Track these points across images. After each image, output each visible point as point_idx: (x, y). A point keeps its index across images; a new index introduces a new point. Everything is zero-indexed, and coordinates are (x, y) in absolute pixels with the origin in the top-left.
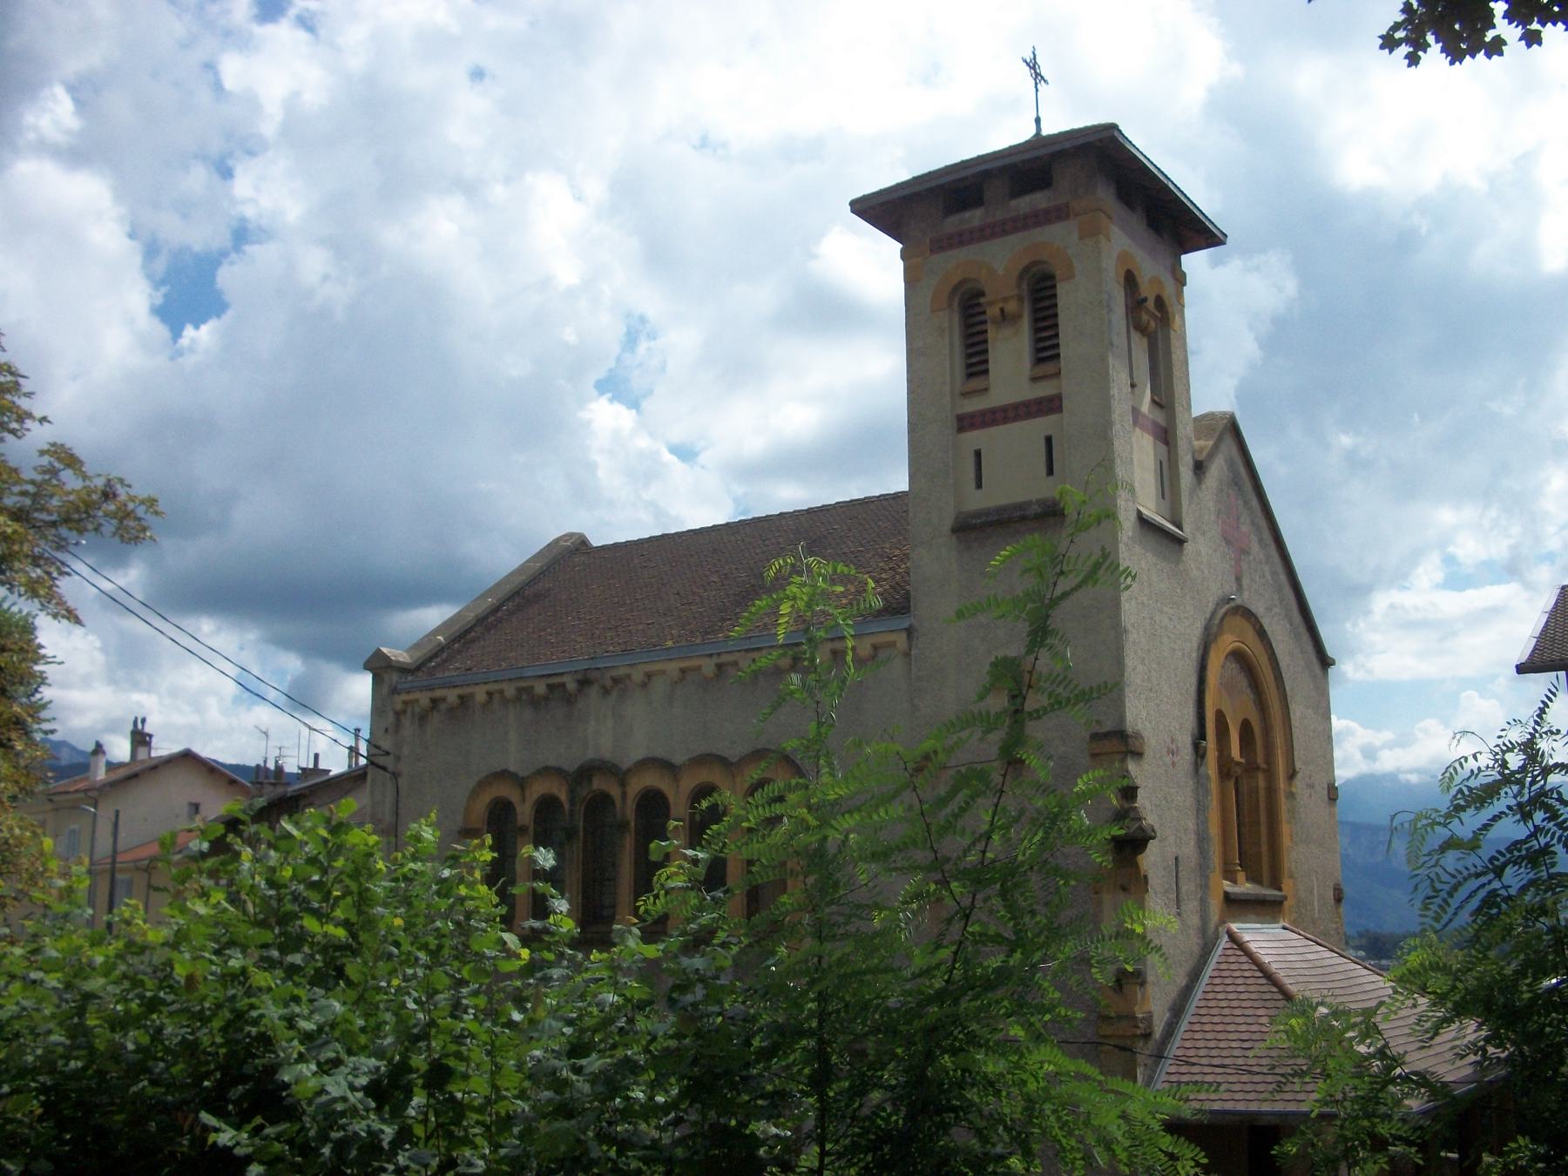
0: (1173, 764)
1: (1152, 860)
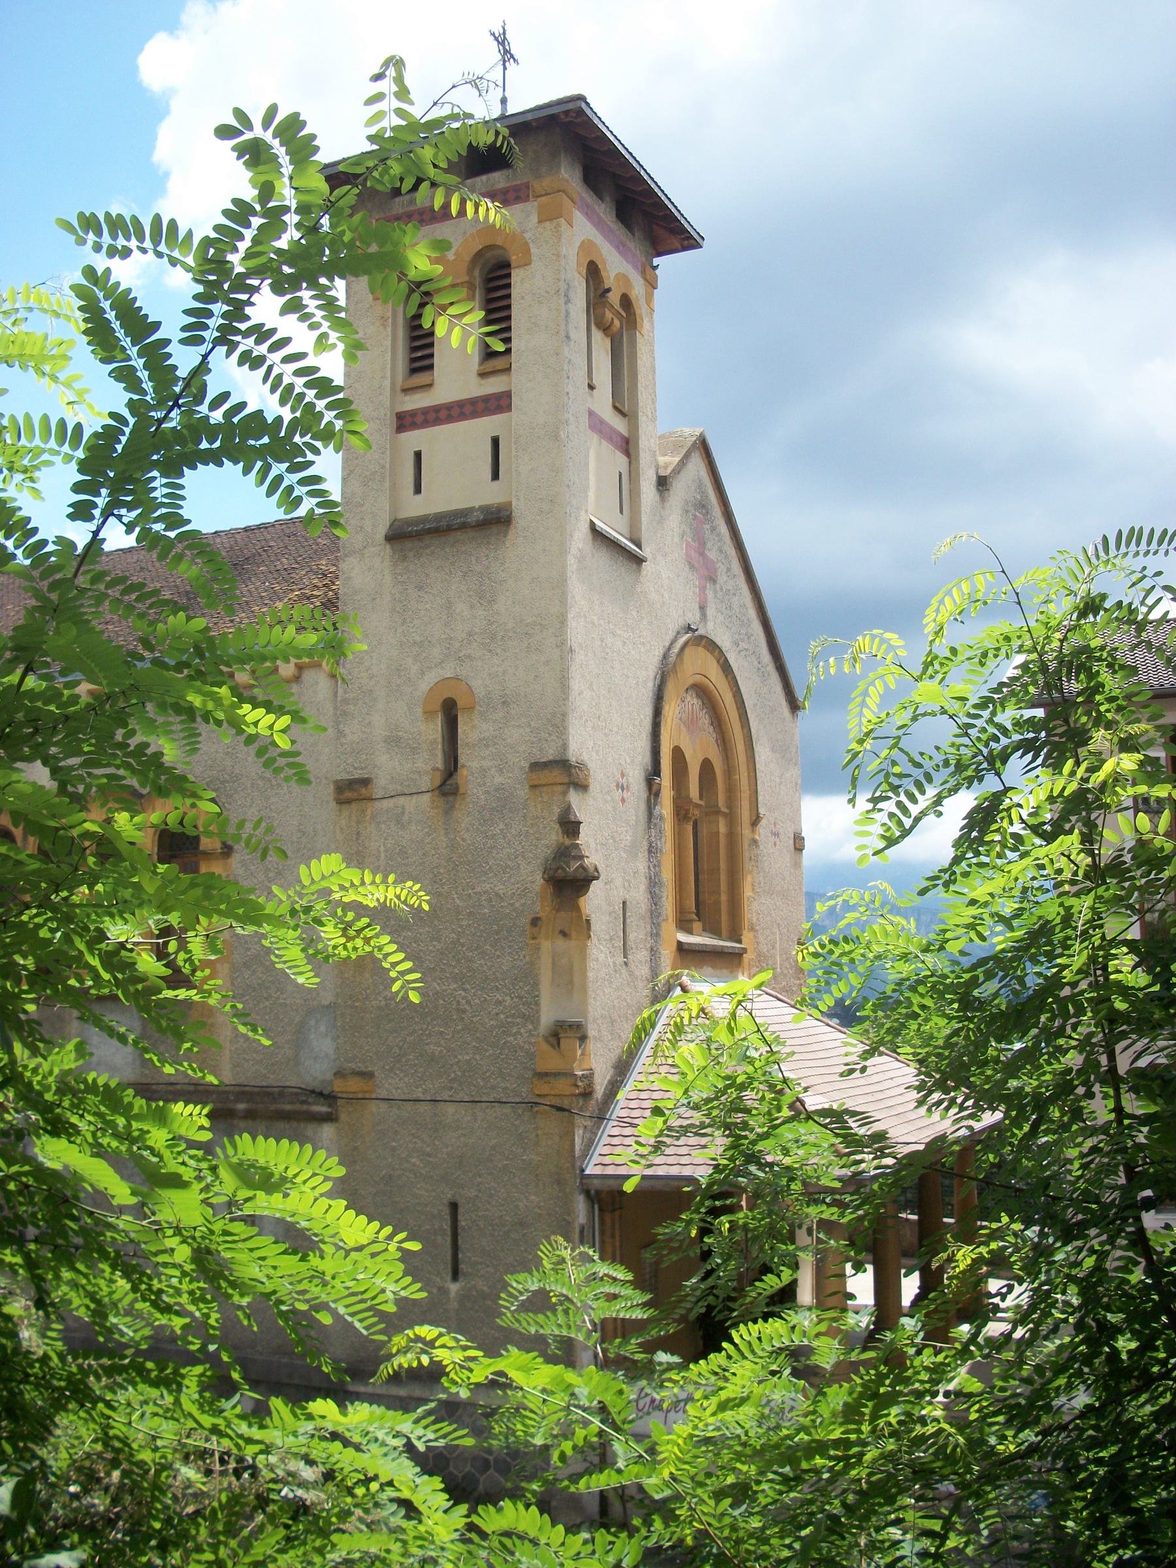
0: (623, 800)
1: (596, 902)
